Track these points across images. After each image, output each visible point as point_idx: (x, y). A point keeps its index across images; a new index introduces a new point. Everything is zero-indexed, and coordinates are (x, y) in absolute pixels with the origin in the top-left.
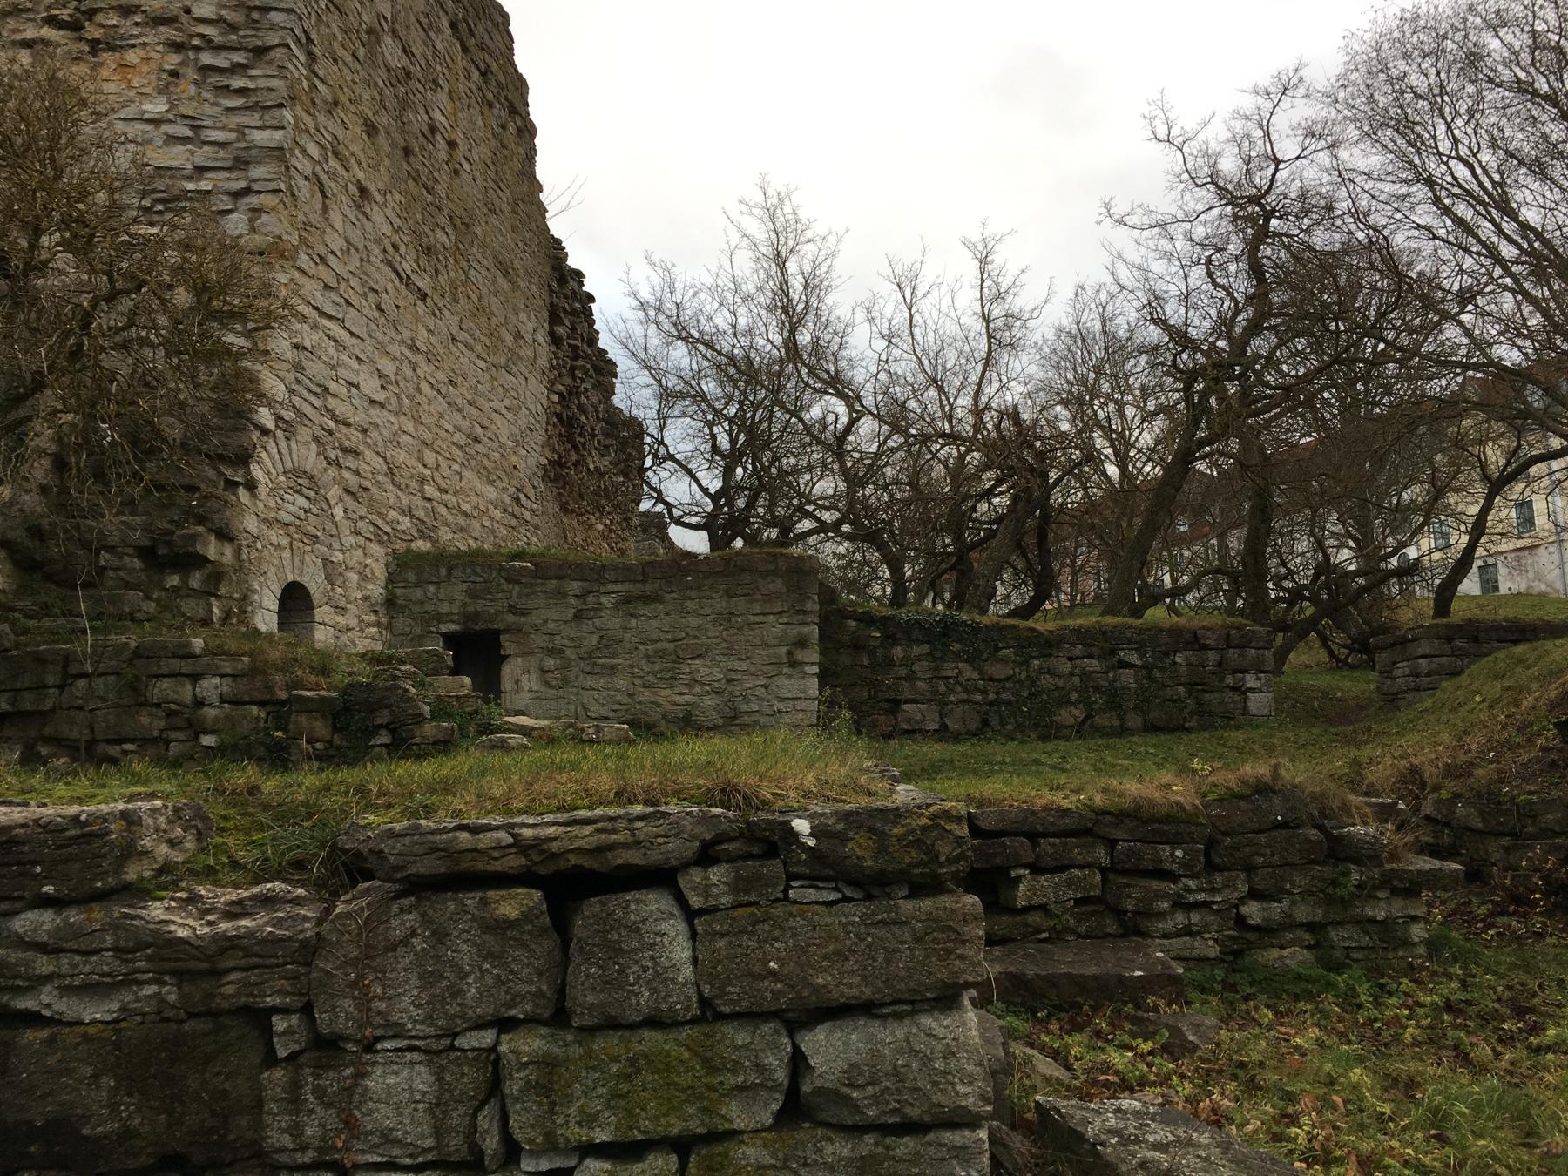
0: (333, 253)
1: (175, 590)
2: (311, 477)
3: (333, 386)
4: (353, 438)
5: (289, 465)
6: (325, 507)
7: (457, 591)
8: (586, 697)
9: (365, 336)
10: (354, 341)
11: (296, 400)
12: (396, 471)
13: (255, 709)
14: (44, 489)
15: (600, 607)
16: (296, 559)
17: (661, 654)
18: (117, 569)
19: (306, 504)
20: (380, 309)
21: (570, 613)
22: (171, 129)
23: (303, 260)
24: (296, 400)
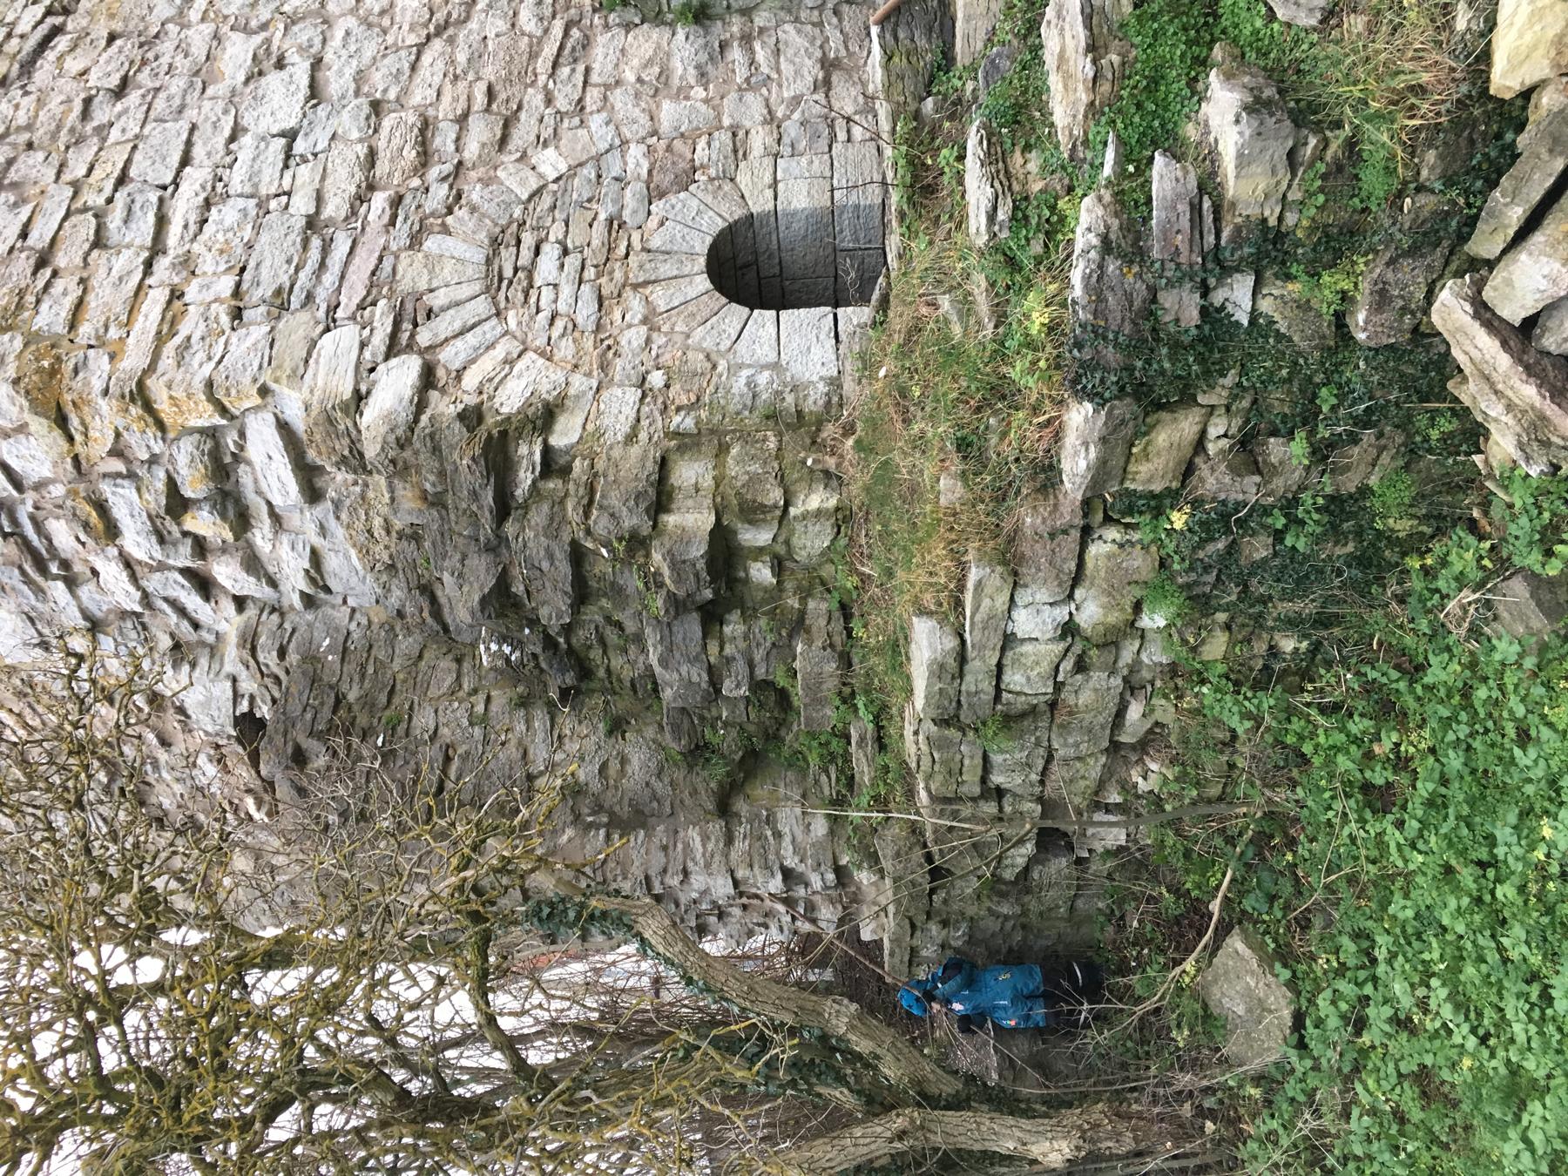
0: (24, 235)
1: (779, 566)
2: (496, 243)
3: (302, 204)
4: (396, 133)
5: (482, 306)
6: (547, 200)
9: (184, 126)
10: (198, 152)
11: (349, 302)
12: (440, 16)
13: (1095, 550)
14: (617, 727)
16: (666, 269)
18: (751, 665)
19: (550, 252)
20: (120, 92)
23: (50, 317)
24: (349, 302)
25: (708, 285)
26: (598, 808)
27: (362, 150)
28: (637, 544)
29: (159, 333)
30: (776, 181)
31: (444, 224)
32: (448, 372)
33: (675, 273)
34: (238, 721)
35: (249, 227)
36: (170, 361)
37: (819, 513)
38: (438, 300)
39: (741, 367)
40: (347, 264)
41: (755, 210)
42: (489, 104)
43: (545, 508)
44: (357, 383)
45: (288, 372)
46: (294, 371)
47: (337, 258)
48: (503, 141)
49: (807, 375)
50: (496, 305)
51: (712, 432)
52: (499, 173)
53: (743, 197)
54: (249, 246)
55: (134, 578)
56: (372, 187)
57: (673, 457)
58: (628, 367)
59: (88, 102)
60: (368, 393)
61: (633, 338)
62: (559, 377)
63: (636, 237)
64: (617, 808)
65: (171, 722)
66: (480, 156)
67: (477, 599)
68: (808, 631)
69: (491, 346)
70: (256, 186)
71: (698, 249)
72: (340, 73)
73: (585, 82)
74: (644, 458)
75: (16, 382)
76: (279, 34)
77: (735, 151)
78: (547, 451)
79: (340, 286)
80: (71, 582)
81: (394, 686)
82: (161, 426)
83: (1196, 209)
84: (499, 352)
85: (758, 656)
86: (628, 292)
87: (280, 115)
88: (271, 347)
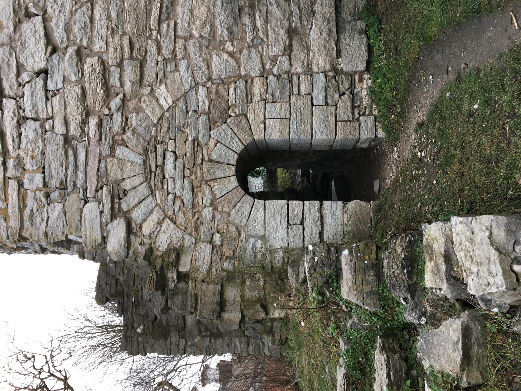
2: (146, 151)
19: (169, 156)
26: (207, 329)
27: (78, 90)
29: (19, 207)
31: (123, 139)
32: (136, 224)
33: (223, 175)
35: (40, 140)
36: (28, 223)
40: (86, 165)
41: (256, 138)
42: (132, 53)
43: (180, 297)
44: (102, 233)
45: (75, 229)
46: (77, 227)
47: (81, 161)
49: (276, 245)
50: (150, 187)
52: (143, 105)
53: (251, 129)
57: (225, 284)
58: (206, 231)
60: (107, 236)
63: (205, 152)
64: (212, 330)
66: (132, 91)
67: (160, 311)
69: (151, 212)
70: (37, 112)
71: (231, 162)
78: (179, 274)
79: (86, 179)
81: (134, 277)
88: (66, 217)
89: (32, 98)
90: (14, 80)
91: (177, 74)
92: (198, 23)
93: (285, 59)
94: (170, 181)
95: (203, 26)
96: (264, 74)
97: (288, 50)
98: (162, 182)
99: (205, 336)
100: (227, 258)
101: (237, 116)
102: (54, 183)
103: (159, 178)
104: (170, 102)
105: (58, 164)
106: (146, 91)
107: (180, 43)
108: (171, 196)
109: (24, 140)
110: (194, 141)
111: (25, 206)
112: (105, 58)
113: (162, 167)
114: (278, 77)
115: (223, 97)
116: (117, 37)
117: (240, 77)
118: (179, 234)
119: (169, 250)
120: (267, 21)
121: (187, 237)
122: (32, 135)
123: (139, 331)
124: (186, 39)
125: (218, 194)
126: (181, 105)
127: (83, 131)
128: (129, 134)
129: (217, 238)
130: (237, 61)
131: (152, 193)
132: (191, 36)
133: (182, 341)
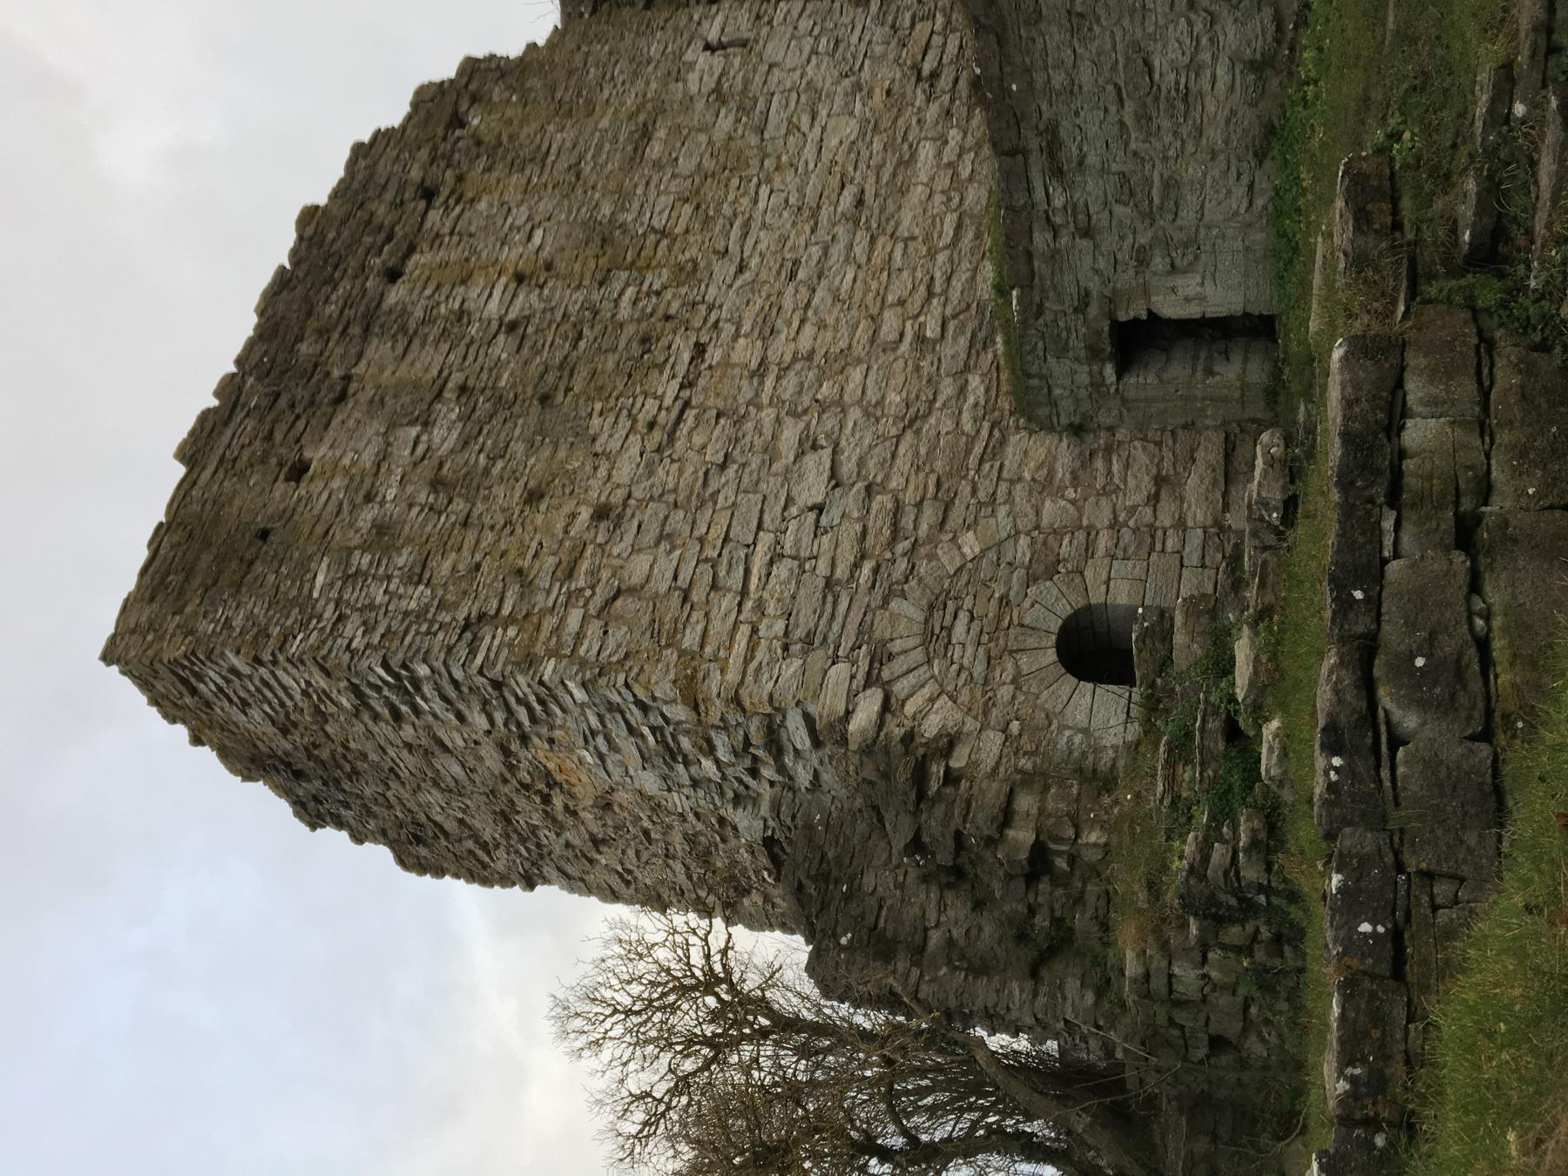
0: (675, 578)
2: (931, 607)
3: (823, 568)
6: (965, 577)
7: (1059, 368)
8: (1213, 213)
9: (759, 497)
15: (1071, 208)
16: (1031, 642)
17: (1144, 118)
19: (963, 617)
21: (1084, 244)
22: (604, 748)
25: (1054, 657)
26: (962, 958)
27: (858, 528)
28: (990, 842)
30: (1109, 579)
34: (765, 839)
37: (1095, 845)
38: (896, 646)
39: (1067, 727)
40: (846, 617)
43: (943, 806)
48: (943, 523)
50: (928, 654)
51: (1042, 774)
52: (939, 552)
54: (794, 597)
55: (719, 768)
56: (863, 557)
57: (1017, 789)
59: (706, 473)
61: (1005, 692)
62: (958, 716)
63: (1015, 614)
65: (729, 832)
68: (1084, 905)
69: (923, 686)
70: (798, 550)
72: (849, 458)
73: (999, 478)
74: (999, 792)
75: (675, 682)
76: (814, 422)
77: (1087, 550)
78: (948, 769)
80: (687, 764)
82: (744, 710)
83: (1226, 873)
84: (926, 692)
85: (1057, 906)
86: (1006, 657)
87: (813, 492)
89: (797, 535)
90: (779, 514)
91: (992, 521)
92: (1032, 464)
93: (1149, 511)
94: (958, 649)
95: (1040, 467)
96: (1115, 525)
97: (1154, 500)
98: (946, 648)
99: (956, 968)
100: (1025, 753)
101: (1068, 572)
102: (799, 633)
103: (942, 643)
104: (977, 550)
105: (809, 612)
106: (946, 537)
107: (1003, 487)
108: (955, 667)
109: (773, 580)
110: (1001, 599)
111: (753, 658)
112: (901, 496)
113: (950, 630)
114: (1135, 531)
115: (1052, 550)
116: (922, 475)
117: (1080, 527)
118: (958, 716)
119: (939, 736)
120: (1127, 466)
121: (969, 720)
122: (784, 574)
123: (844, 941)
124: (1012, 482)
125: (1025, 669)
126: (992, 555)
127: (852, 576)
128: (913, 583)
129: (1015, 727)
130: (1080, 510)
131: (929, 662)
132: (1020, 479)
133: (915, 972)
